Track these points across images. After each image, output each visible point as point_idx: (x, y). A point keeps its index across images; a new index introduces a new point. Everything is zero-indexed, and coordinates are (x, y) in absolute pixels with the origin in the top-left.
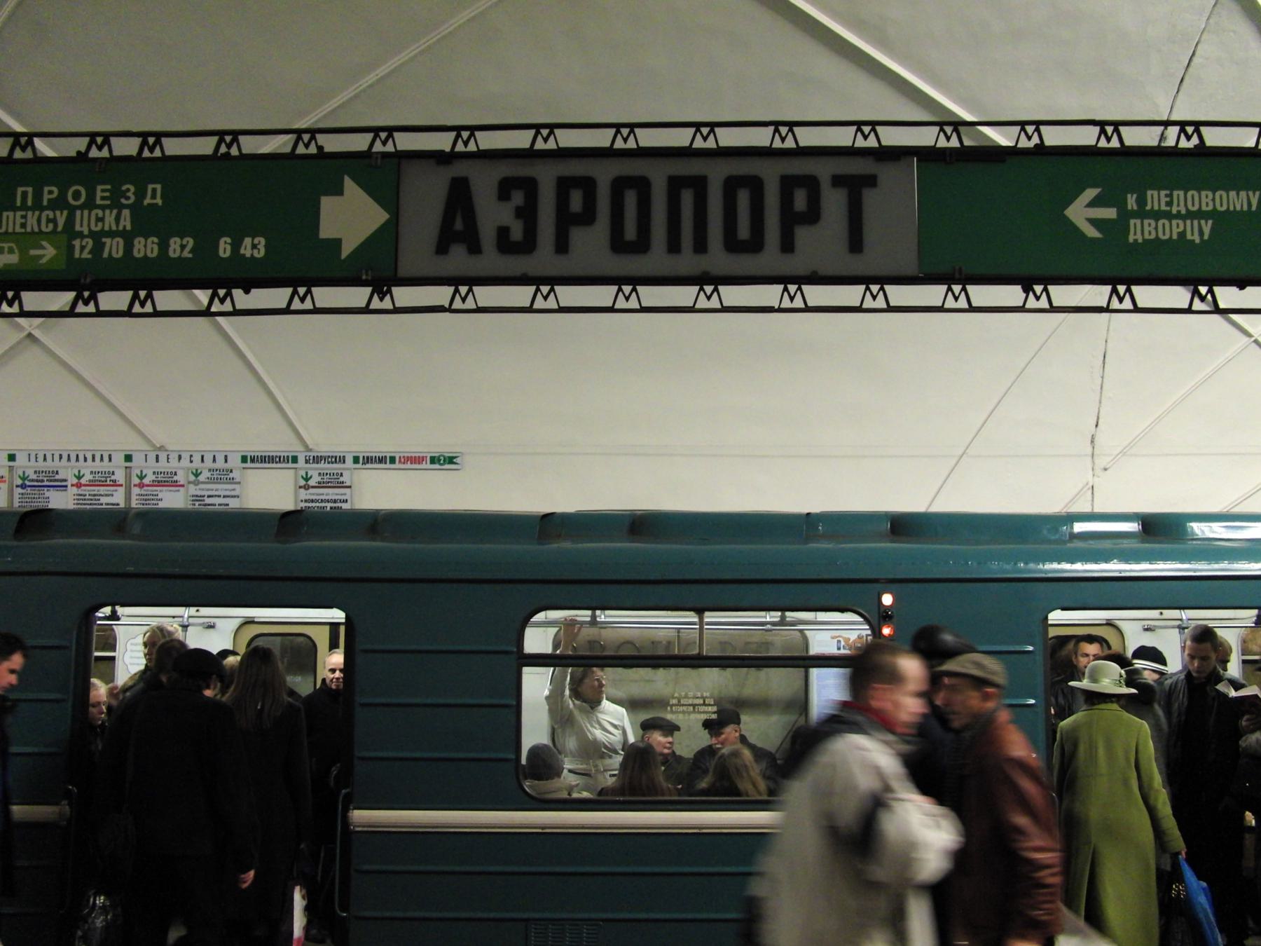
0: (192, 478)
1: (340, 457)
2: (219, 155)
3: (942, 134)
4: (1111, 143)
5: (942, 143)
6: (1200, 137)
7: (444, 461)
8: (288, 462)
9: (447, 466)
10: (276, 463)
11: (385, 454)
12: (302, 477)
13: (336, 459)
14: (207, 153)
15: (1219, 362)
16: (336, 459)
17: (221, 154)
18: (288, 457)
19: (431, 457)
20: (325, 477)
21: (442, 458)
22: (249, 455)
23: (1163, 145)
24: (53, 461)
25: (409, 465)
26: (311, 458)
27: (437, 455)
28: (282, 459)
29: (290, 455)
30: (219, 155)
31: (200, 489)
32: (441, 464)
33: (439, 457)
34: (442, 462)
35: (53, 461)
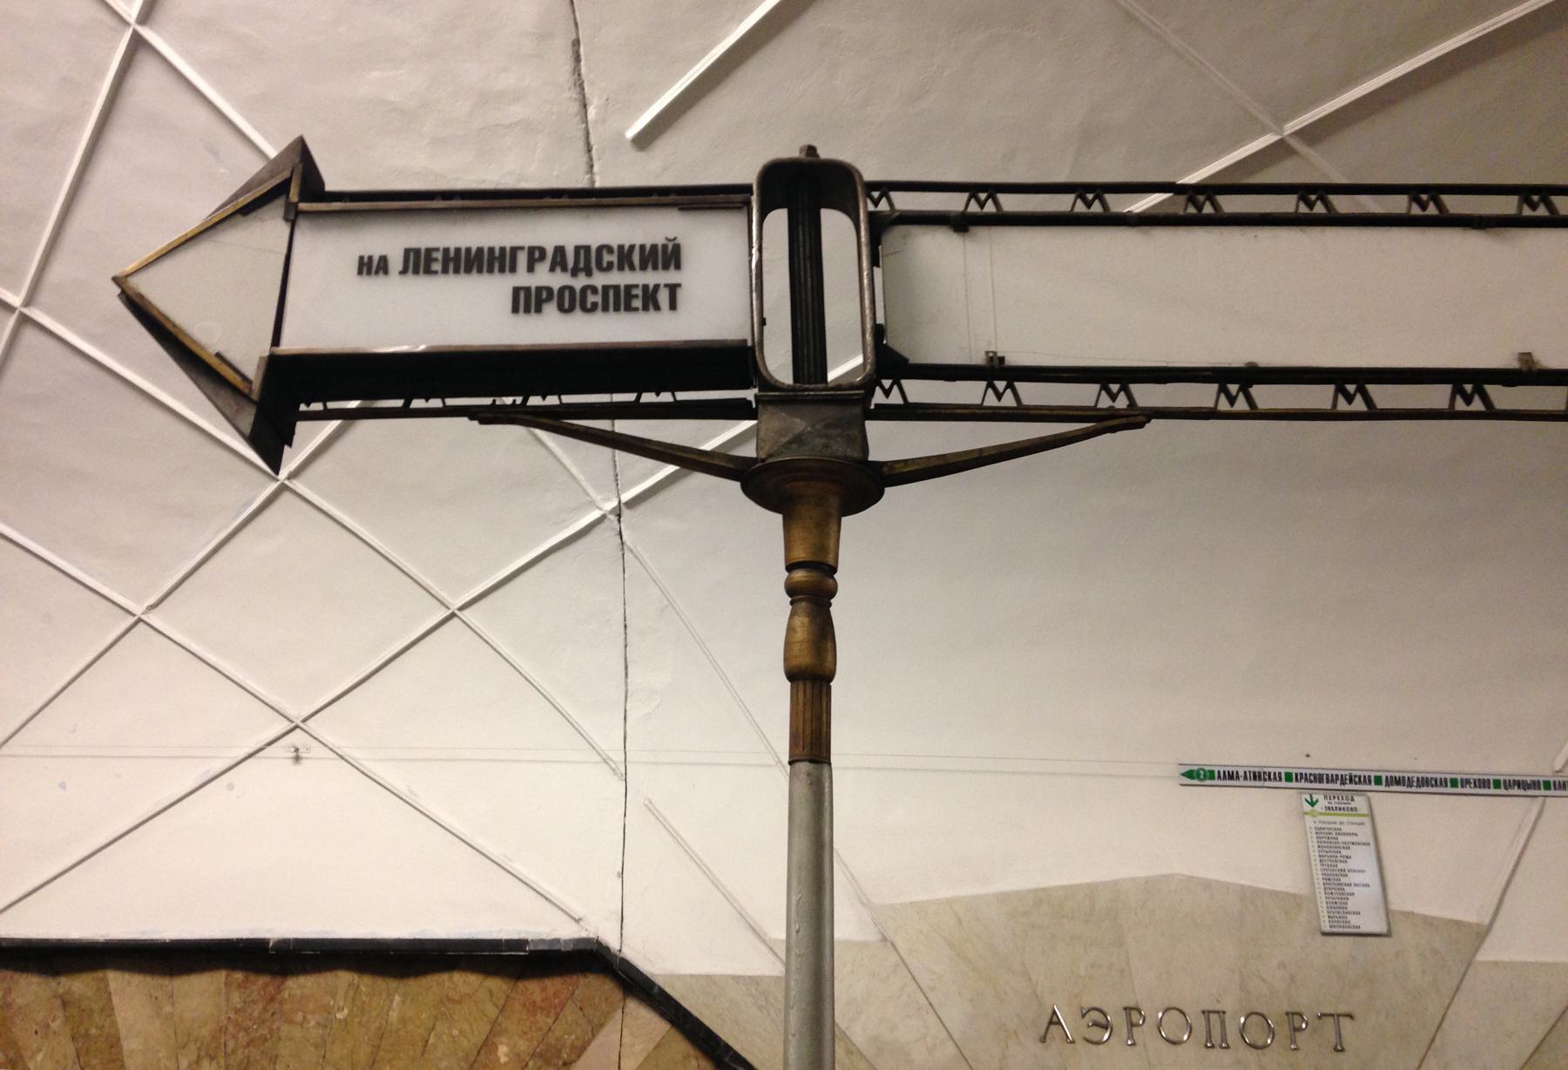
0: (1307, 807)
1: (1275, 773)
2: (872, 407)
3: (990, 391)
4: (1354, 404)
5: (1105, 402)
6: (1130, 396)
7: (1204, 776)
8: (1446, 786)
9: (1208, 782)
10: (1356, 784)
11: (1369, 773)
12: (1306, 800)
13: (1360, 779)
14: (417, 400)
15: (486, 632)
16: (1360, 779)
17: (876, 405)
18: (1280, 773)
19: (1375, 777)
20: (1333, 801)
21: (1202, 772)
22: (1294, 771)
23: (255, 397)
24: (1196, 776)
25: (1516, 791)
26: (1415, 779)
27: (1196, 768)
28: (1272, 777)
29: (1449, 777)
30: (872, 407)
31: (1320, 822)
32: (1200, 779)
33: (1198, 771)
34: (1202, 777)
35: (1196, 776)
